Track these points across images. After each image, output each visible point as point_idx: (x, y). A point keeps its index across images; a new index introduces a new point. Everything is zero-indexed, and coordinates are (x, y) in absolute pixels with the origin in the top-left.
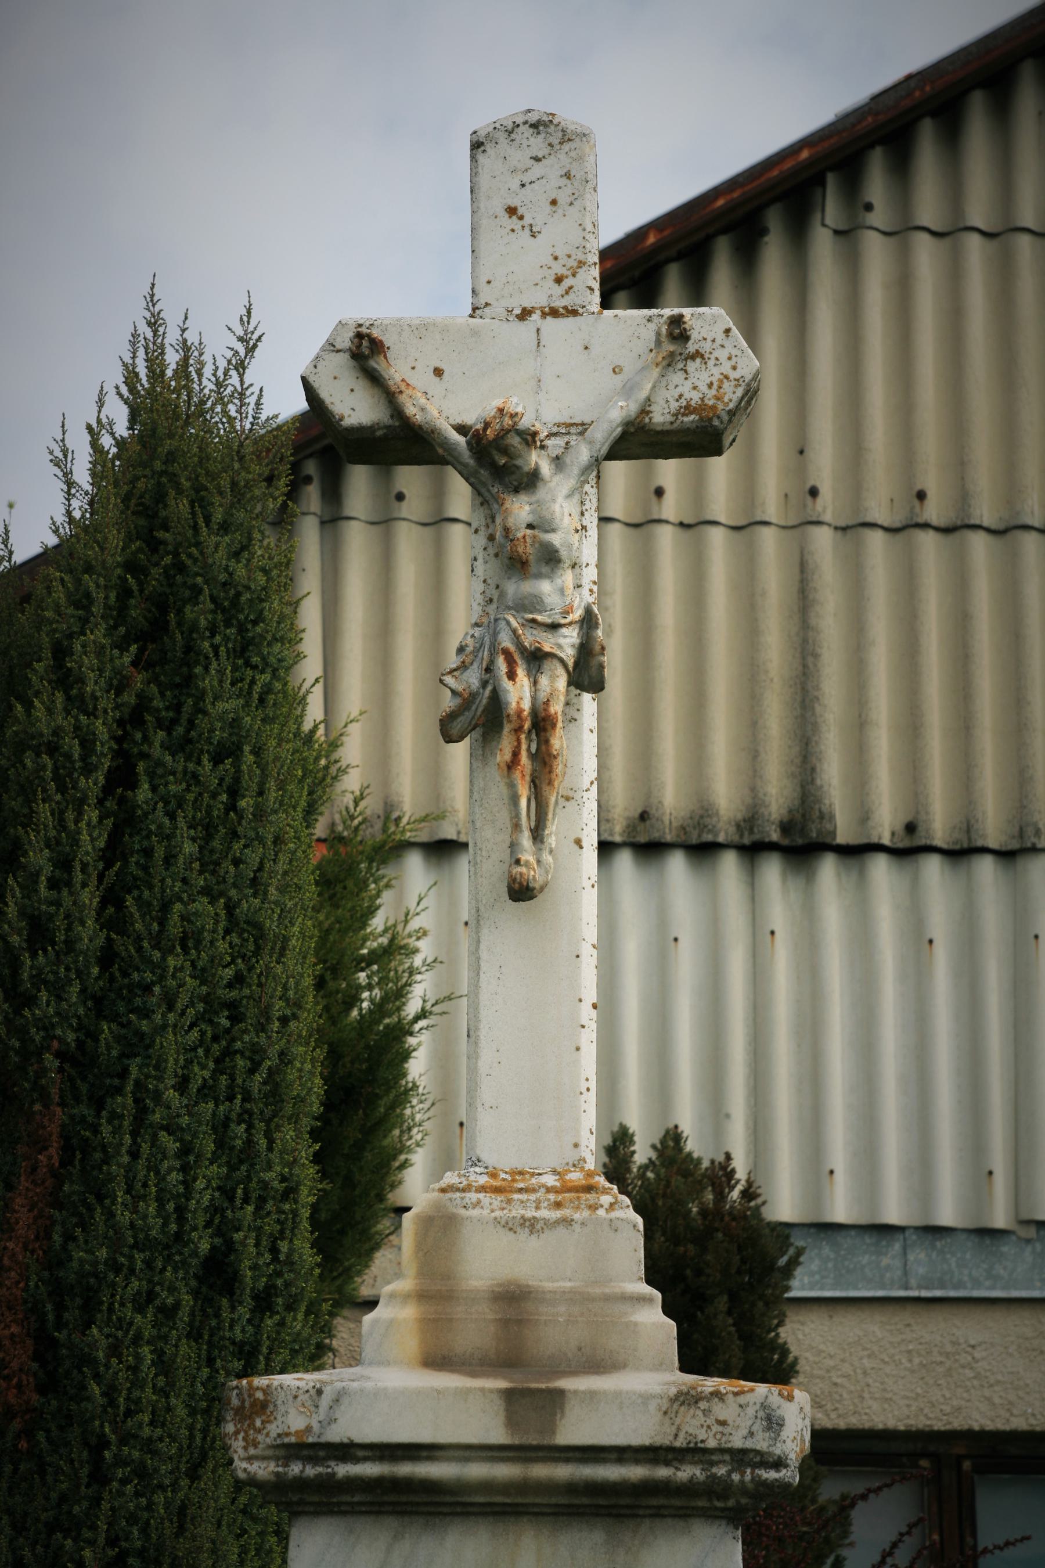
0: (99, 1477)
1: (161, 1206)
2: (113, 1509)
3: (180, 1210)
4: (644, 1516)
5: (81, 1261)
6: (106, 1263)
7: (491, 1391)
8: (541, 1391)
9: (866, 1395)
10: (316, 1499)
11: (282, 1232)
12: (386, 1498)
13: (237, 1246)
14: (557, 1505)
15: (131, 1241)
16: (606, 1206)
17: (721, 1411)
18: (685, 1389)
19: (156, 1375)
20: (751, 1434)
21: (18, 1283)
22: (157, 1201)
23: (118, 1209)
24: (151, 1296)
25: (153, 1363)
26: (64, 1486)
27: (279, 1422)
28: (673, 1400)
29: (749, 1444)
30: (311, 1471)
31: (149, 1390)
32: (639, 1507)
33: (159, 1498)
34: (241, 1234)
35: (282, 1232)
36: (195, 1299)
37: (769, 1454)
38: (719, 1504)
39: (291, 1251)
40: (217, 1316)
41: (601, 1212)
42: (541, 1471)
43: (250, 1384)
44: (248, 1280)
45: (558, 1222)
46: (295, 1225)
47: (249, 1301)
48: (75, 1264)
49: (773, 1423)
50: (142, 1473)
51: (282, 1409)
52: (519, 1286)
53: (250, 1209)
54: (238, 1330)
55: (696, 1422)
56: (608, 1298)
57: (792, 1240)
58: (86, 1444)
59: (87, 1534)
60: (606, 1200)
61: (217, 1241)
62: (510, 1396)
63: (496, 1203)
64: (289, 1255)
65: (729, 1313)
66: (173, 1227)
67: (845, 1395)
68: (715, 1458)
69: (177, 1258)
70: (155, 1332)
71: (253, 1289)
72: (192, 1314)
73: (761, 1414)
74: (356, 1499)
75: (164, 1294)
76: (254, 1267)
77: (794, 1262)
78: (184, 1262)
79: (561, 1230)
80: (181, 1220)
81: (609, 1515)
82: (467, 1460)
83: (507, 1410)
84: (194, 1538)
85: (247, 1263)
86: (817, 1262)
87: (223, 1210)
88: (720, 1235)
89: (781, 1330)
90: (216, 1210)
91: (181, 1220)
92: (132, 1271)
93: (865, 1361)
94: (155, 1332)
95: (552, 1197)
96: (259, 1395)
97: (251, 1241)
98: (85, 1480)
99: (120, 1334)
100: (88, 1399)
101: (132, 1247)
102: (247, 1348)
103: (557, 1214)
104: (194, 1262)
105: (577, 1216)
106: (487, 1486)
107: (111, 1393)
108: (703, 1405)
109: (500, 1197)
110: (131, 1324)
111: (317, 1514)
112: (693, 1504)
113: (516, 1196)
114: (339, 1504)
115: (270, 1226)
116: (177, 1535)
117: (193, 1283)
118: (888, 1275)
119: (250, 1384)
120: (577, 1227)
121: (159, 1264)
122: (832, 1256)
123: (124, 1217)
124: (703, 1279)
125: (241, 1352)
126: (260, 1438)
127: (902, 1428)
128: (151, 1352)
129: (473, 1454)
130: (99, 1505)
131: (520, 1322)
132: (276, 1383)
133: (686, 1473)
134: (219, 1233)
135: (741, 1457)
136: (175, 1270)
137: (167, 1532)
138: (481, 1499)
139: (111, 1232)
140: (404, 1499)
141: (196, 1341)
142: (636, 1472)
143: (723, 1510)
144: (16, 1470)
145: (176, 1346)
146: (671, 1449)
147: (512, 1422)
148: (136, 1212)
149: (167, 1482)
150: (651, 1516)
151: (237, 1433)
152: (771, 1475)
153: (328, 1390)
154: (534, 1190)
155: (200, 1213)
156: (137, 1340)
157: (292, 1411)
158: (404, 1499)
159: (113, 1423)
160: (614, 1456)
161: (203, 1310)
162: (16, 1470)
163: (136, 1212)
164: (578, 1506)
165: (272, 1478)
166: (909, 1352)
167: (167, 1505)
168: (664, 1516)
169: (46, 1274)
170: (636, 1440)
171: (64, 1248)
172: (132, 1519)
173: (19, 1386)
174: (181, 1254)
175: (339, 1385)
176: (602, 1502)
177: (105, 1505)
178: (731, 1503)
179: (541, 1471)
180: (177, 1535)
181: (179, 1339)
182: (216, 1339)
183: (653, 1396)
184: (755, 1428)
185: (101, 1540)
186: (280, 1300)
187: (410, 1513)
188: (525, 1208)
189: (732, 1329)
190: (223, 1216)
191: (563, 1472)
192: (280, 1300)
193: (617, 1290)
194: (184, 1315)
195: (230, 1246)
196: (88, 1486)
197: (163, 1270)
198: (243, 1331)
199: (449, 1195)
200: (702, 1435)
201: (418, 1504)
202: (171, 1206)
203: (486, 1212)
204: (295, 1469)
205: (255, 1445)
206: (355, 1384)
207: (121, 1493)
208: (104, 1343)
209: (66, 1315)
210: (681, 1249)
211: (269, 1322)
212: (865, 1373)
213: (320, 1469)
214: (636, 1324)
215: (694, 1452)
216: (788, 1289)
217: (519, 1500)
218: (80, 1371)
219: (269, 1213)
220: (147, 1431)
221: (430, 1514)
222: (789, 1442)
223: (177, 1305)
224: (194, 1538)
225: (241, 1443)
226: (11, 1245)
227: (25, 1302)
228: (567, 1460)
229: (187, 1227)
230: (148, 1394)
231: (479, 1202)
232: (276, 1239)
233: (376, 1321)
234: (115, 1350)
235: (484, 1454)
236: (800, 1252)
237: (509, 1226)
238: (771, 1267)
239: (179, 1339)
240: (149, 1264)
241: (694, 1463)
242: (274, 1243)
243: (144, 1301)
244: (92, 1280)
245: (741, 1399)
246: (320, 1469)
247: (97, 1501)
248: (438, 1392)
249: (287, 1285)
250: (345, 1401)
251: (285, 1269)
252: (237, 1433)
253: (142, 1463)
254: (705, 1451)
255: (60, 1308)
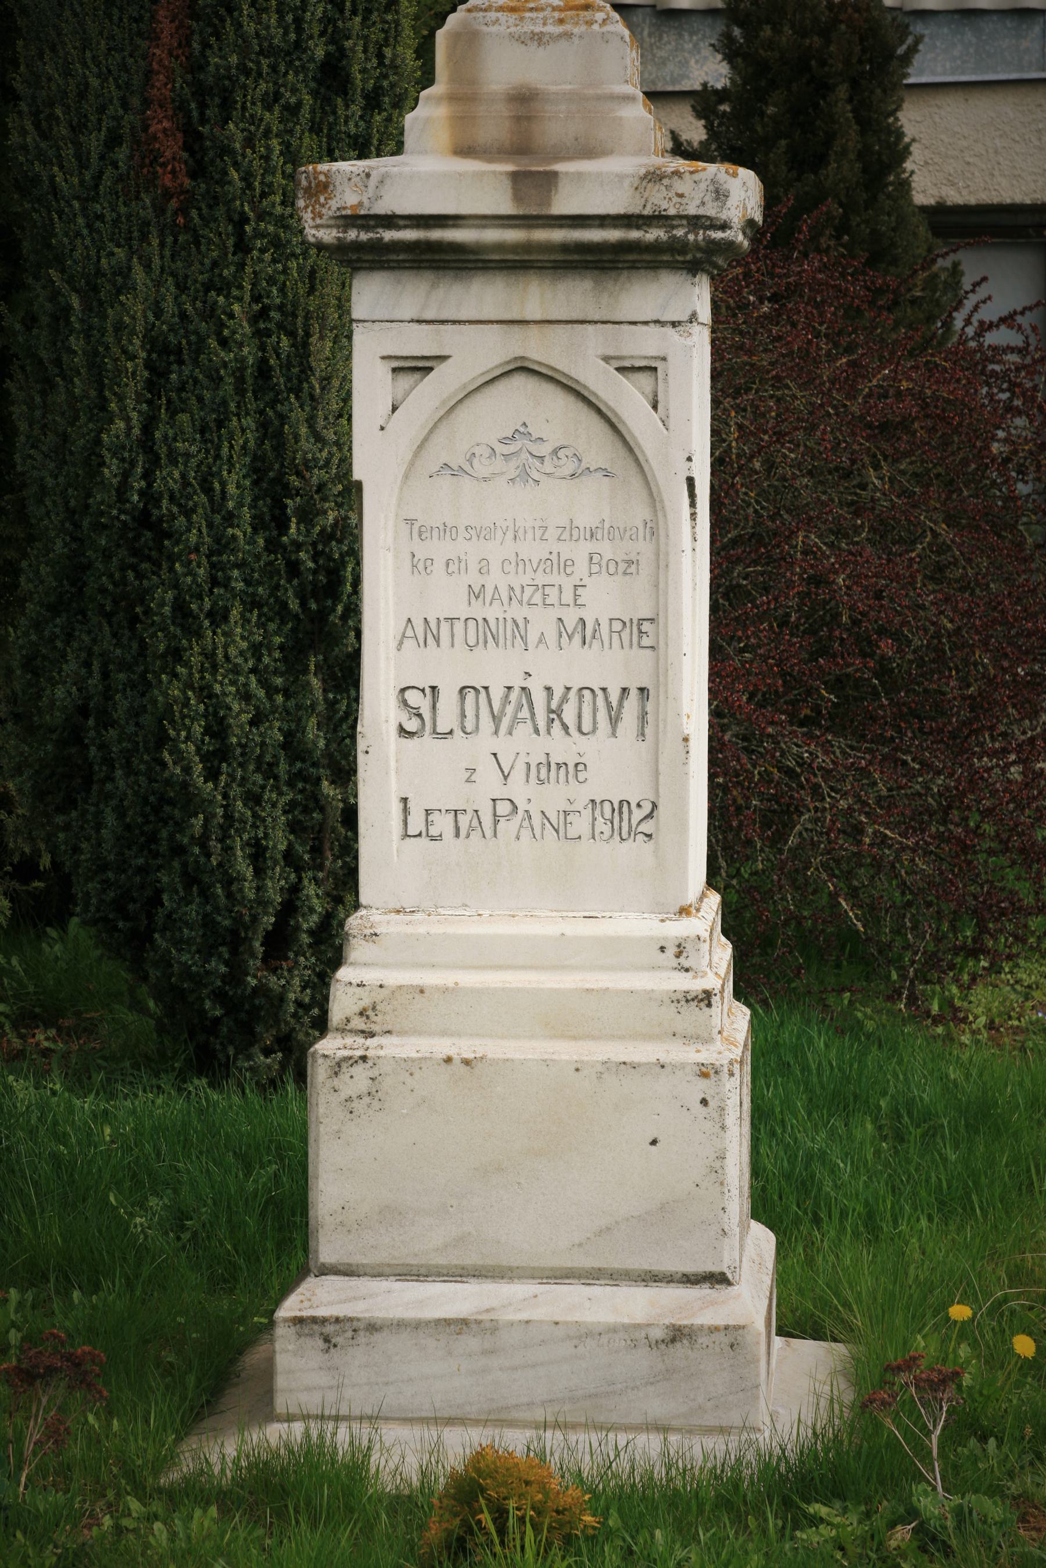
0: (242, 247)
1: (281, 18)
2: (254, 272)
3: (298, 21)
4: (623, 268)
5: (217, 67)
6: (237, 68)
7: (501, 173)
8: (539, 172)
9: (996, 173)
10: (370, 257)
11: (386, 39)
12: (423, 257)
13: (348, 53)
14: (555, 261)
15: (257, 48)
16: (600, 21)
17: (680, 186)
18: (652, 169)
19: (285, 163)
20: (703, 203)
21: (166, 84)
22: (277, 13)
23: (245, 21)
24: (277, 96)
25: (281, 153)
26: (215, 254)
27: (337, 199)
28: (643, 178)
29: (701, 212)
30: (364, 236)
31: (279, 176)
32: (619, 261)
33: (293, 264)
34: (351, 42)
35: (386, 39)
36: (315, 99)
37: (717, 219)
38: (680, 258)
39: (395, 56)
40: (334, 113)
41: (596, 27)
42: (541, 235)
43: (314, 169)
44: (358, 82)
45: (560, 36)
46: (398, 34)
47: (360, 101)
48: (211, 68)
49: (720, 195)
50: (277, 243)
51: (339, 188)
52: (529, 89)
53: (358, 19)
54: (351, 124)
55: (660, 196)
56: (599, 98)
57: (911, 28)
58: (230, 220)
59: (235, 292)
60: (600, 16)
61: (331, 48)
62: (516, 177)
63: (511, 21)
64: (393, 60)
65: (850, 100)
66: (293, 36)
67: (977, 174)
68: (675, 223)
69: (297, 63)
70: (282, 127)
71: (363, 90)
72: (313, 111)
73: (711, 188)
74: (401, 257)
75: (287, 95)
76: (364, 71)
77: (913, 50)
78: (303, 67)
79: (563, 43)
80: (299, 30)
81: (596, 268)
82: (484, 227)
83: (513, 188)
84: (322, 296)
85: (357, 67)
86: (959, 47)
87: (335, 21)
88: (843, 27)
89: (900, 114)
90: (329, 21)
91: (299, 30)
92: (260, 74)
93: (997, 141)
94: (282, 127)
95: (556, 14)
96: (322, 178)
97: (359, 48)
98: (231, 249)
99: (252, 128)
100: (230, 183)
101: (259, 54)
102: (360, 140)
103: (559, 29)
104: (312, 66)
105: (576, 30)
106: (500, 247)
107: (247, 178)
108: (666, 182)
109: (515, 16)
110: (261, 120)
111: (371, 269)
112: (659, 258)
113: (528, 15)
114: (388, 261)
115: (376, 35)
116: (309, 294)
117: (313, 85)
118: (1027, 58)
119: (314, 169)
120: (576, 40)
121: (283, 69)
122: (974, 40)
123: (250, 28)
124: (826, 69)
125: (355, 144)
126: (324, 211)
127: (1028, 202)
128: (280, 144)
129: (488, 222)
130: (243, 269)
131: (529, 118)
132: (334, 169)
133: (653, 234)
134: (333, 41)
135: (695, 222)
136: (296, 73)
137: (301, 292)
138: (497, 257)
139: (240, 41)
140: (437, 257)
141: (318, 135)
142: (613, 235)
143: (683, 262)
144: (176, 241)
145: (300, 139)
146: (640, 217)
147: (518, 197)
148: (260, 23)
149: (298, 251)
150: (628, 268)
151: (306, 207)
152: (718, 235)
153: (374, 174)
154: (542, 9)
155: (315, 24)
156: (267, 133)
157: (348, 190)
158: (437, 257)
159: (251, 202)
160: (597, 222)
161: (322, 108)
162: (176, 241)
163: (260, 23)
164: (572, 262)
165: (335, 241)
166: (1039, 131)
167: (300, 269)
168: (638, 268)
169: (189, 77)
170: (613, 210)
171: (202, 53)
172: (271, 281)
173: (173, 172)
174: (300, 59)
175: (383, 170)
176: (589, 258)
177: (248, 270)
178: (689, 257)
179: (541, 235)
180: (309, 294)
181: (303, 132)
182: (334, 132)
183: (627, 176)
184: (706, 199)
185: (247, 298)
186: (386, 99)
187: (444, 268)
188: (535, 24)
189: (850, 115)
190: (335, 26)
191: (558, 235)
192: (386, 99)
193: (607, 91)
194: (305, 112)
195: (342, 52)
196: (234, 254)
197: (286, 73)
198: (356, 126)
199: (474, 14)
200: (664, 205)
201: (449, 261)
202: (289, 18)
203: (503, 28)
204: (352, 235)
205: (321, 216)
206: (396, 169)
207: (260, 260)
208: (239, 136)
209: (208, 112)
210: (808, 41)
211: (378, 118)
212: (996, 152)
213: (371, 235)
214: (621, 118)
215: (658, 219)
216: (906, 75)
217: (526, 257)
218: (222, 160)
219: (374, 23)
220: (279, 210)
221: (459, 269)
222: (733, 209)
223: (299, 104)
224: (322, 296)
225: (310, 215)
226: (157, 52)
227: (173, 101)
228: (561, 226)
229: (304, 36)
230: (279, 179)
231: (498, 20)
232: (381, 46)
233: (416, 119)
234: (249, 142)
235: (496, 222)
236: (918, 40)
237: (521, 40)
238: (891, 56)
239: (303, 132)
240: (274, 68)
241: (660, 227)
242: (380, 49)
243: (271, 101)
244: (227, 82)
245: (696, 177)
246: (371, 235)
247: (241, 266)
248: (460, 175)
249: (393, 86)
250: (388, 182)
251: (390, 72)
252: (306, 207)
253: (277, 236)
254: (667, 218)
255: (202, 106)
